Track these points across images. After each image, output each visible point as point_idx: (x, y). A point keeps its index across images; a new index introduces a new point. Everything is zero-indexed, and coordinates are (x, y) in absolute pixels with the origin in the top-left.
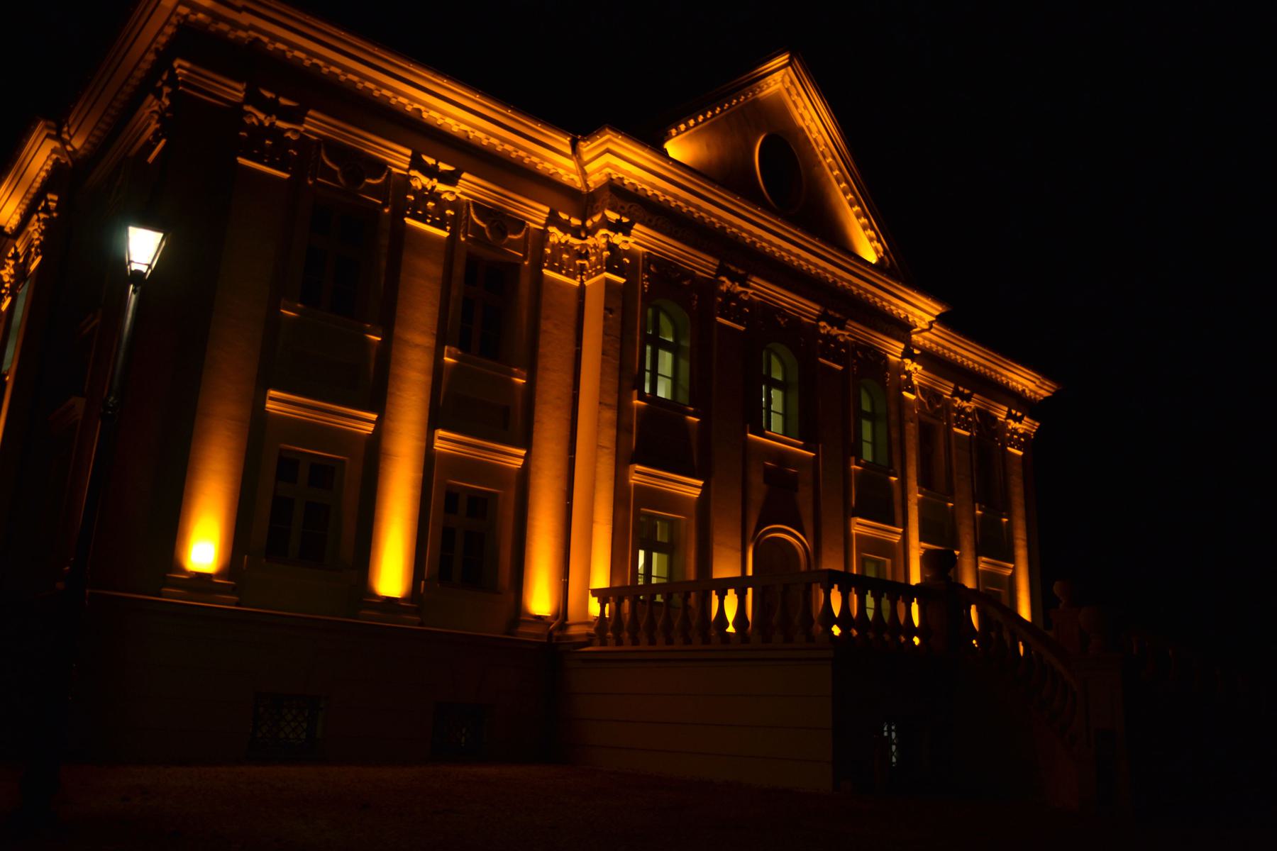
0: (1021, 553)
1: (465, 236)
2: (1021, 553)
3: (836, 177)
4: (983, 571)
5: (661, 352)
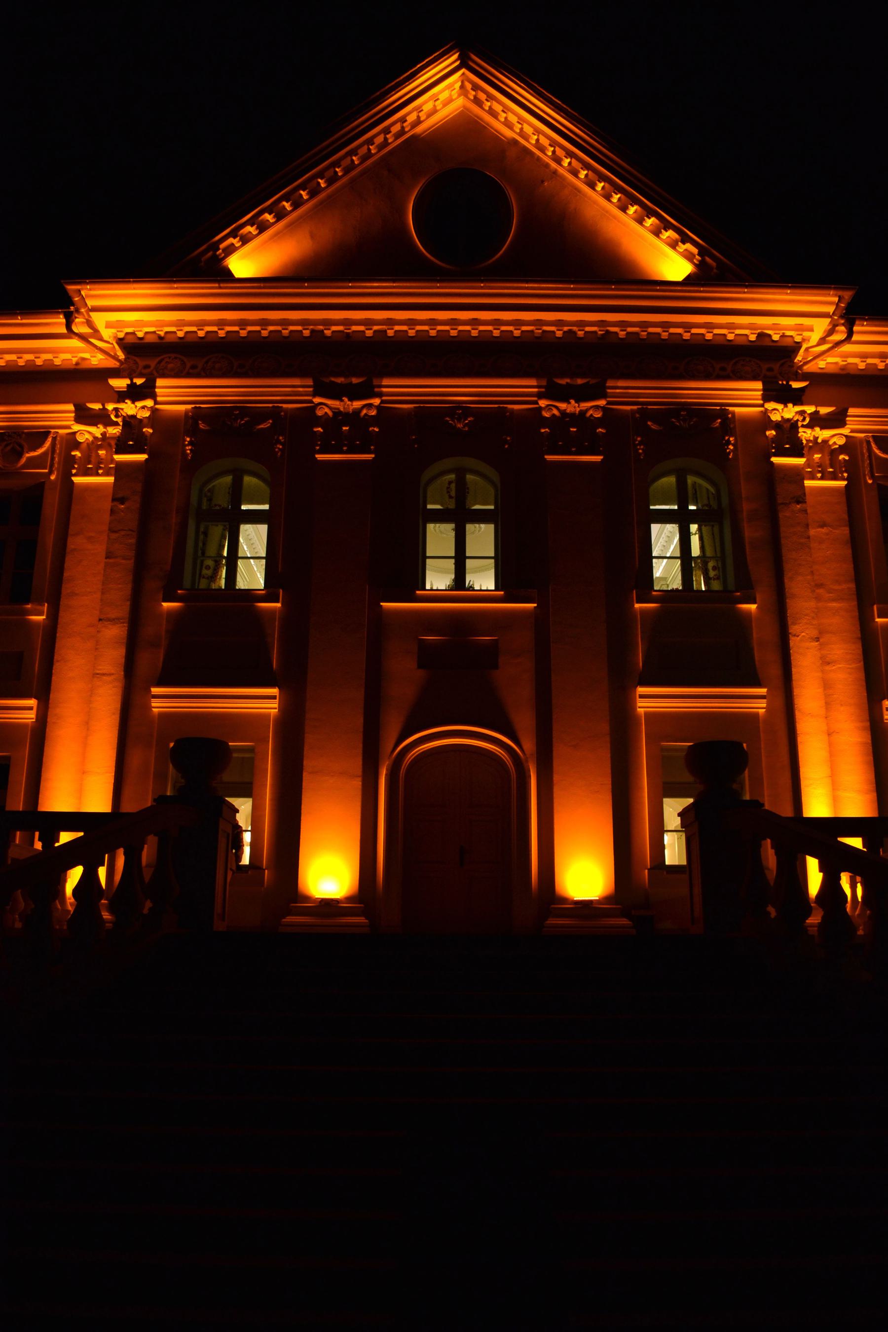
1: (872, 477)
3: (330, 182)
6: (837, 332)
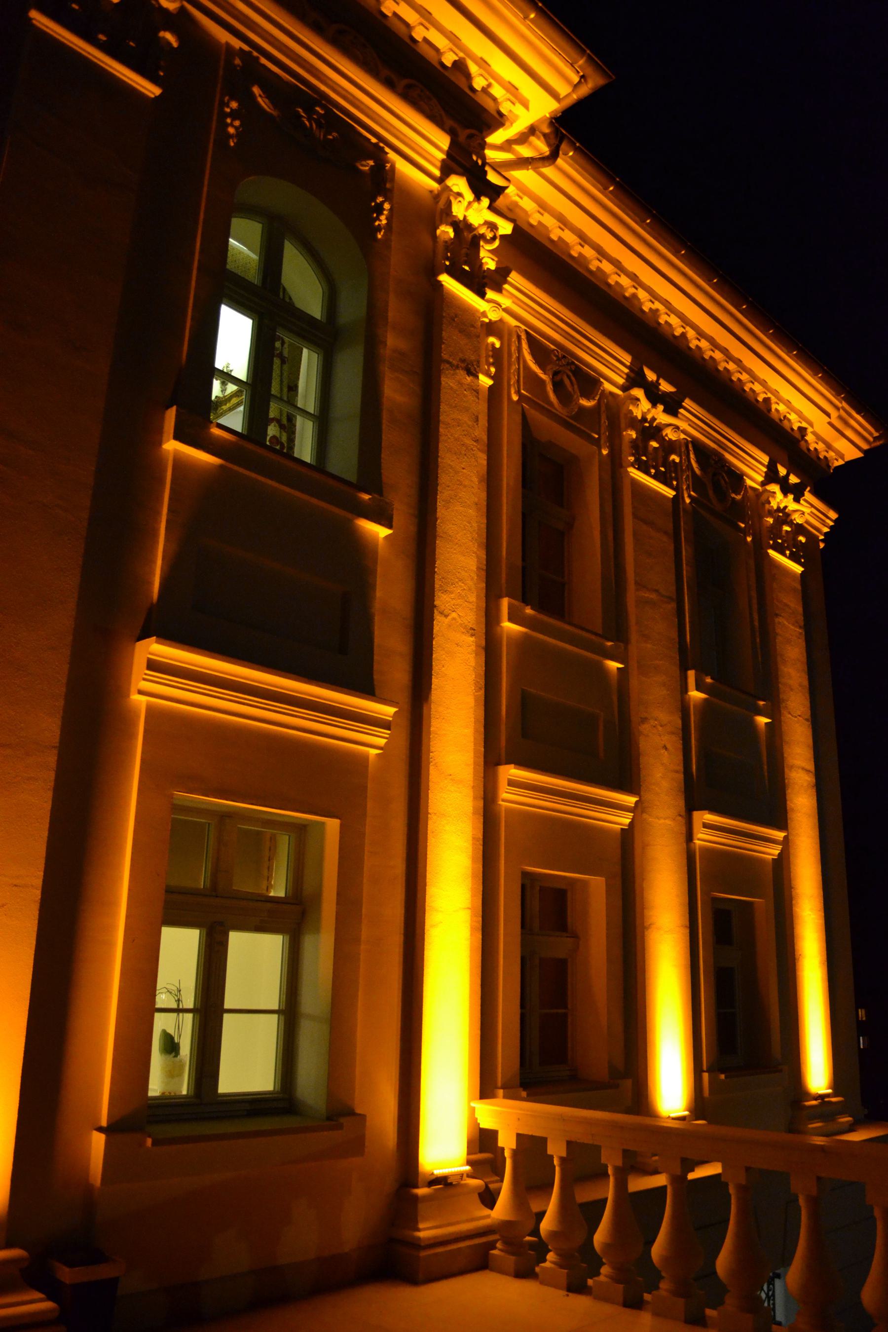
0: (802, 803)
1: (518, 392)
2: (802, 803)
4: (705, 851)
5: (238, 941)
6: (531, 144)
